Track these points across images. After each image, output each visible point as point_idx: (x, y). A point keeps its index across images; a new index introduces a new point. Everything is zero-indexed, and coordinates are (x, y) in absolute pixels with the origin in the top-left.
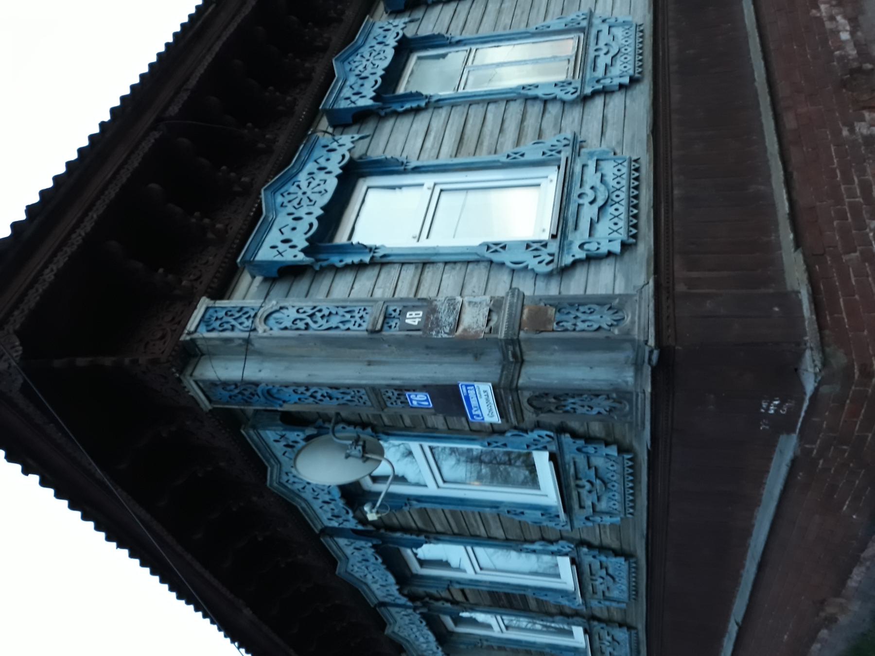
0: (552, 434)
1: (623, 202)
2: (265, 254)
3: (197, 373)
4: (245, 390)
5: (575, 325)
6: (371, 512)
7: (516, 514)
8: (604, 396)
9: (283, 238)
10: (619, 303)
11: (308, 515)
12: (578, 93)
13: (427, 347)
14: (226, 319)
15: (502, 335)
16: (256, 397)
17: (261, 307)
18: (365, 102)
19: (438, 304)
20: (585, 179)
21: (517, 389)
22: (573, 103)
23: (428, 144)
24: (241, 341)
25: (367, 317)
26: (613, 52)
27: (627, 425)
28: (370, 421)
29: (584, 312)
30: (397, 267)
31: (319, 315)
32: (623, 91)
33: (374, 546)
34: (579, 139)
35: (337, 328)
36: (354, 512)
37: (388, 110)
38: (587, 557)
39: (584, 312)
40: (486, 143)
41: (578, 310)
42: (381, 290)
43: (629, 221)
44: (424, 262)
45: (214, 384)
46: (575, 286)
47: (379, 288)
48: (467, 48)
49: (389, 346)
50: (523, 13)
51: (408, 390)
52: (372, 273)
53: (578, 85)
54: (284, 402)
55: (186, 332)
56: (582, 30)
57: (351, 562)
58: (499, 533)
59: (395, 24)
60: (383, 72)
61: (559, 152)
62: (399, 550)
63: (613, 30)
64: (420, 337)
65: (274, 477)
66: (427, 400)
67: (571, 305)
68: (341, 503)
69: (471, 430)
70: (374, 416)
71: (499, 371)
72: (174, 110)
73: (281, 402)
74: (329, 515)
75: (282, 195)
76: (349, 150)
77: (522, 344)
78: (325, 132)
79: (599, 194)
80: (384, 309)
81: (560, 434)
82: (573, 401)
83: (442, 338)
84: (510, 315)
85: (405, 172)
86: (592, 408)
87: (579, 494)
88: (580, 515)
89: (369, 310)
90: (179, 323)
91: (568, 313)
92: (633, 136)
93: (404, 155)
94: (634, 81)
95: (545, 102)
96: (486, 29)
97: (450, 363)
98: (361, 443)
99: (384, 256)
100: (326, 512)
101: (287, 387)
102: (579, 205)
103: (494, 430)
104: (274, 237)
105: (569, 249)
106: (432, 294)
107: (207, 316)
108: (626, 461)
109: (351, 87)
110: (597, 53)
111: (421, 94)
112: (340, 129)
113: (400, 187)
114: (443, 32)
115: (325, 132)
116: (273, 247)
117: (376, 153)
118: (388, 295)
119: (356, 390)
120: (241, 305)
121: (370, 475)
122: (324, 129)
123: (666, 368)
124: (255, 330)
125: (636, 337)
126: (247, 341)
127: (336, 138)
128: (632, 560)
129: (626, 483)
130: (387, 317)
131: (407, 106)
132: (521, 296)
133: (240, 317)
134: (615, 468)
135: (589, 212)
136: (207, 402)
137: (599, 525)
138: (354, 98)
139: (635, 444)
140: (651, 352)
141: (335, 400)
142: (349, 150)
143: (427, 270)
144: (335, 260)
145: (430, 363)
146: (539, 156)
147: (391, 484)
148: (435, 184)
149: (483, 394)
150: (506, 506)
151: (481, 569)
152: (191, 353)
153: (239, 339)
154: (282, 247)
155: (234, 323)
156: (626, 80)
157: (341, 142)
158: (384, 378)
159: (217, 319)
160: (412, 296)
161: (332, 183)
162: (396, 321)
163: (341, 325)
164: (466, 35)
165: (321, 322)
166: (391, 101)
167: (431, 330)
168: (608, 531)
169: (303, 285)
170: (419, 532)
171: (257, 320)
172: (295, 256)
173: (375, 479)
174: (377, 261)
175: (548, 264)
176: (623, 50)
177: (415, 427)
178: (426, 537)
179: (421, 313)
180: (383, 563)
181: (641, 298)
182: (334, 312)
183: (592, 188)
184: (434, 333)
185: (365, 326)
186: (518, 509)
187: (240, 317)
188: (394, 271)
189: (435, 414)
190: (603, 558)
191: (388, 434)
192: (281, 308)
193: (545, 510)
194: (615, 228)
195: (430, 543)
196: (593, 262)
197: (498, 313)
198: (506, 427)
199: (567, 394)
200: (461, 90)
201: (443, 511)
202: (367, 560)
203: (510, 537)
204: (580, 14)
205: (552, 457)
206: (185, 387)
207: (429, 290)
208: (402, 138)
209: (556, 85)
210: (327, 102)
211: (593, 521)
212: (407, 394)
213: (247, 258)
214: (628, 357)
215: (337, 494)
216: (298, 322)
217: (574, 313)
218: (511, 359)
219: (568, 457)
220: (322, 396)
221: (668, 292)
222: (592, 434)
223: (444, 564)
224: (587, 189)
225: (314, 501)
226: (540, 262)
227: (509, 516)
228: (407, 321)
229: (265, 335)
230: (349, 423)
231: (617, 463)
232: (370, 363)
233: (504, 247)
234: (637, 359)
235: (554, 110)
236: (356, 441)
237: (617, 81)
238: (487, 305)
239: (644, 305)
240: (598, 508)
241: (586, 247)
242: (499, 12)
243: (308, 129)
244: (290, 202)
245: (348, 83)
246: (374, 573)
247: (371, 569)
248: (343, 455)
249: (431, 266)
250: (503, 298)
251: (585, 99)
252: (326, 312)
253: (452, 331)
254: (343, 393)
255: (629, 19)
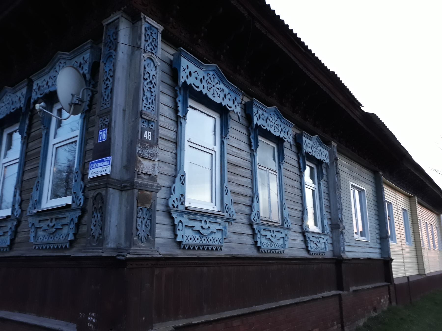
0: (81, 205)
1: (201, 242)
2: (184, 62)
3: (123, 20)
4: (113, 44)
5: (140, 218)
6: (40, 106)
7: (37, 186)
8: (101, 232)
9: (192, 73)
10: (150, 240)
11: (40, 73)
12: (254, 222)
13: (131, 141)
14: (151, 38)
15: (136, 180)
16: (108, 49)
17: (157, 57)
18: (255, 120)
19: (155, 149)
20: (214, 224)
21: (107, 187)
22: (250, 219)
23: (234, 149)
24: (139, 44)
25: (149, 111)
26: (273, 239)
27: (85, 245)
28: (92, 108)
29: (146, 222)
30: (175, 129)
31: (151, 86)
32: (254, 243)
33: (21, 108)
34: (232, 222)
35: (144, 95)
36: (41, 98)
37: (251, 131)
38: (11, 225)
39: (146, 222)
40: (234, 178)
41: (148, 219)
42: (163, 120)
43: (192, 245)
44: (177, 143)
45: (117, 28)
46: (160, 218)
47: (165, 119)
48: (277, 171)
49: (133, 121)
50: (292, 197)
51: (108, 130)
52: (173, 116)
53: (258, 222)
54: (105, 64)
55: (146, 16)
56: (283, 225)
57: (12, 95)
58: (26, 177)
59: (290, 137)
60: (268, 130)
61: (227, 212)
62: (17, 122)
63: (282, 239)
64: (138, 138)
65: (63, 56)
66: (102, 140)
67: (151, 216)
68: (47, 91)
69: (85, 163)
70: (95, 112)
71: (117, 178)
72: (258, 25)
73: (105, 62)
74: (40, 84)
75: (213, 75)
76: (233, 111)
77: (131, 191)
78: (242, 100)
79: (206, 231)
80: (153, 120)
81: (81, 210)
82: (99, 216)
83: (136, 149)
84: (147, 185)
85: (222, 137)
86: (94, 226)
87: (48, 220)
88: (35, 221)
89: (153, 112)
90: (150, 13)
91: (146, 215)
92: (233, 248)
93: (230, 137)
94: (258, 248)
95: (251, 206)
96: (285, 180)
97: (123, 153)
98: (80, 103)
99: (181, 123)
100: (42, 82)
101: (113, 66)
102: (201, 221)
103: (84, 175)
104: (193, 68)
105: (180, 216)
106: (160, 146)
107: (153, 29)
108: (65, 244)
109: (263, 114)
110: (272, 231)
111: (257, 147)
112: (243, 107)
113: (215, 134)
114: (285, 160)
115: (242, 100)
116: (187, 66)
117: (231, 124)
118: (161, 123)
119: (109, 102)
120: (158, 46)
121: (62, 108)
122: (244, 99)
123: (116, 265)
124: (145, 52)
125: (132, 248)
126: (139, 48)
127: (239, 105)
128: (8, 249)
129: (53, 245)
130: (149, 121)
131: (252, 141)
132: (157, 191)
133: (152, 45)
134: (61, 239)
135: (197, 226)
136: (107, 23)
137: (29, 231)
138: (257, 115)
139: (74, 249)
140: (123, 256)
141: (104, 90)
142: (233, 111)
143: (173, 144)
144: (180, 98)
145: (123, 142)
146: (225, 202)
147: (57, 118)
148: (215, 151)
149: (104, 169)
150: (42, 181)
151: (6, 167)
152: (134, 19)
153: (141, 43)
154: (187, 71)
155: (149, 42)
156: (259, 245)
157: (237, 107)
158: (115, 117)
159: (152, 33)
160: (160, 135)
161: (218, 100)
162: (147, 126)
163: (145, 97)
164: (283, 170)
165: (148, 87)
166: (255, 133)
167: (141, 144)
168: (26, 236)
169: (168, 81)
170: (29, 134)
171: (150, 54)
172: (182, 77)
173: (60, 112)
174: (179, 120)
175: (173, 205)
176: (273, 244)
177: (88, 133)
178: (25, 137)
179: (150, 139)
180: (11, 113)
181: (152, 251)
182: (153, 94)
183: (209, 227)
184: (139, 145)
185: (144, 109)
186: (40, 188)
187: (152, 45)
188: (173, 127)
189: (94, 144)
190: (9, 233)
191: (84, 118)
192: (156, 67)
193: (39, 202)
194: (189, 239)
195: (22, 139)
196: (172, 227)
197: (148, 179)
198: (86, 181)
199: (102, 213)
200: (258, 166)
201: (40, 147)
202: (12, 104)
203: (24, 183)
204: (290, 224)
205: (68, 206)
206: (116, 12)
207: (163, 145)
208: (238, 137)
209: (258, 211)
210: (256, 102)
211: (31, 227)
212: (106, 129)
213: (182, 53)
214: (122, 245)
215: (52, 89)
216: (148, 75)
217: (146, 217)
218: (123, 185)
219: (68, 214)
220: (107, 84)
221: (155, 264)
222: (80, 227)
223: (9, 146)
224: (209, 225)
225: (48, 77)
226: (174, 201)
227: (36, 182)
228: (146, 132)
229: (142, 57)
230: (92, 98)
231: (64, 239)
232: (124, 111)
233: (182, 183)
234: (120, 249)
235: (247, 210)
236: (81, 100)
237: (259, 240)
238: (153, 174)
239: (149, 252)
240: (38, 230)
241: (180, 224)
242: (293, 187)
243: (244, 91)
244: (210, 78)
245: (264, 113)
246: (5, 107)
247: (7, 106)
248: (73, 93)
249: (175, 147)
250: (156, 182)
251: (251, 225)
252: (153, 90)
253: (139, 154)
254: (108, 95)
255: (287, 247)
